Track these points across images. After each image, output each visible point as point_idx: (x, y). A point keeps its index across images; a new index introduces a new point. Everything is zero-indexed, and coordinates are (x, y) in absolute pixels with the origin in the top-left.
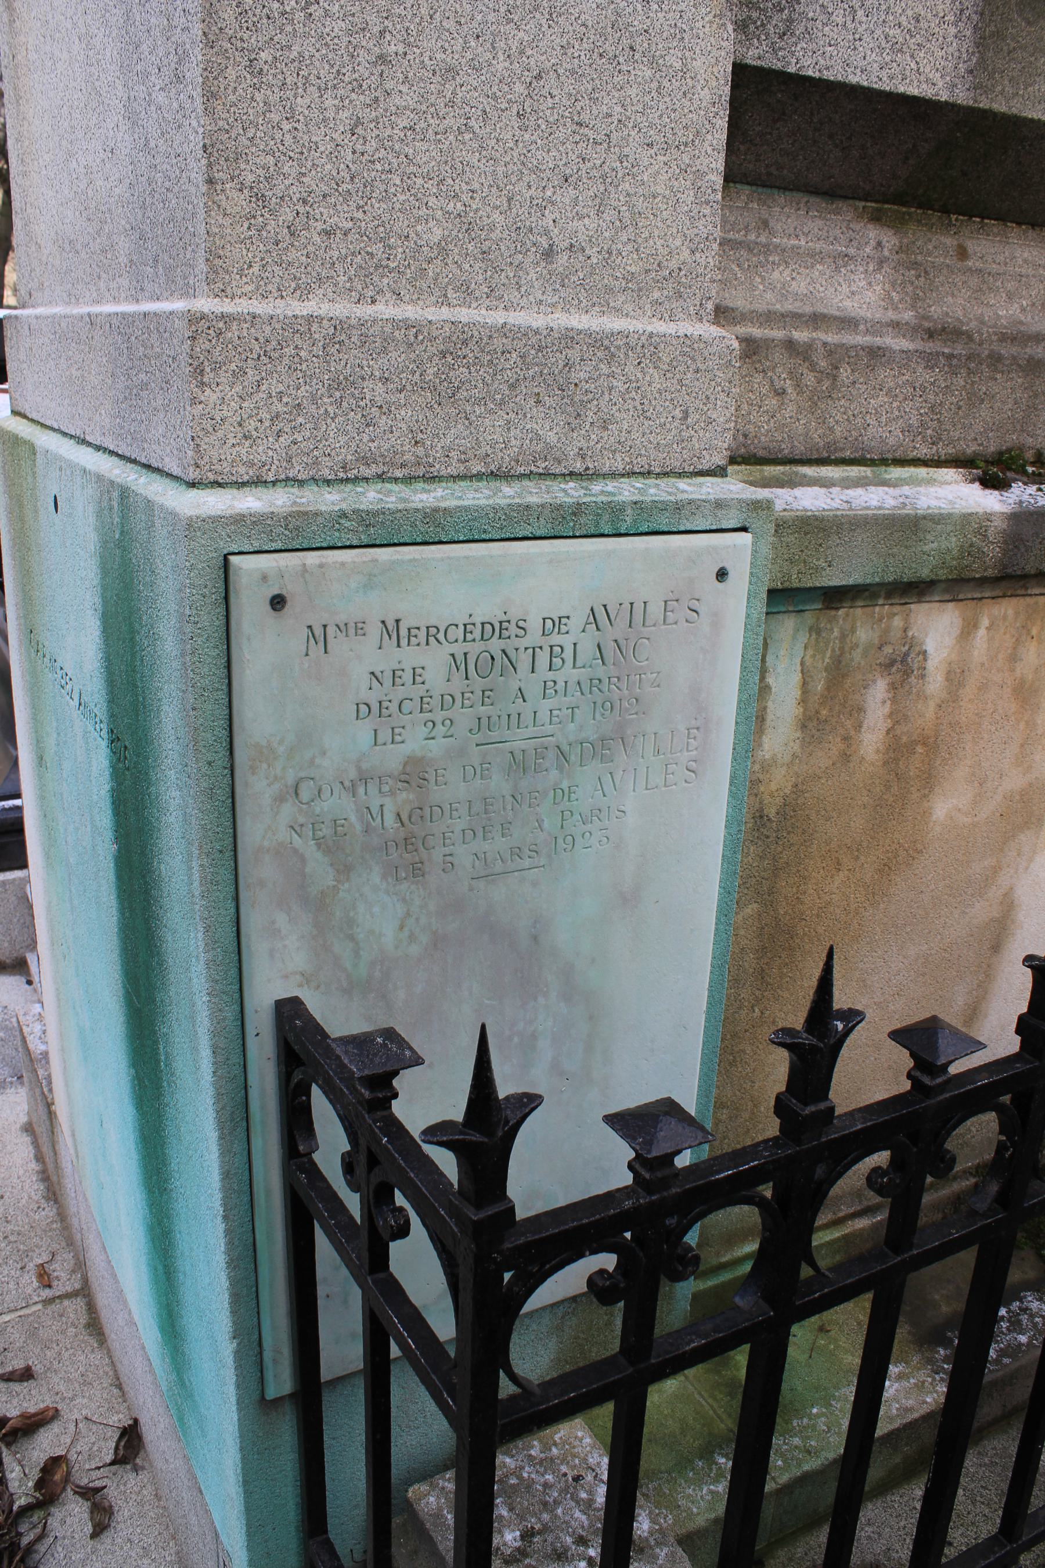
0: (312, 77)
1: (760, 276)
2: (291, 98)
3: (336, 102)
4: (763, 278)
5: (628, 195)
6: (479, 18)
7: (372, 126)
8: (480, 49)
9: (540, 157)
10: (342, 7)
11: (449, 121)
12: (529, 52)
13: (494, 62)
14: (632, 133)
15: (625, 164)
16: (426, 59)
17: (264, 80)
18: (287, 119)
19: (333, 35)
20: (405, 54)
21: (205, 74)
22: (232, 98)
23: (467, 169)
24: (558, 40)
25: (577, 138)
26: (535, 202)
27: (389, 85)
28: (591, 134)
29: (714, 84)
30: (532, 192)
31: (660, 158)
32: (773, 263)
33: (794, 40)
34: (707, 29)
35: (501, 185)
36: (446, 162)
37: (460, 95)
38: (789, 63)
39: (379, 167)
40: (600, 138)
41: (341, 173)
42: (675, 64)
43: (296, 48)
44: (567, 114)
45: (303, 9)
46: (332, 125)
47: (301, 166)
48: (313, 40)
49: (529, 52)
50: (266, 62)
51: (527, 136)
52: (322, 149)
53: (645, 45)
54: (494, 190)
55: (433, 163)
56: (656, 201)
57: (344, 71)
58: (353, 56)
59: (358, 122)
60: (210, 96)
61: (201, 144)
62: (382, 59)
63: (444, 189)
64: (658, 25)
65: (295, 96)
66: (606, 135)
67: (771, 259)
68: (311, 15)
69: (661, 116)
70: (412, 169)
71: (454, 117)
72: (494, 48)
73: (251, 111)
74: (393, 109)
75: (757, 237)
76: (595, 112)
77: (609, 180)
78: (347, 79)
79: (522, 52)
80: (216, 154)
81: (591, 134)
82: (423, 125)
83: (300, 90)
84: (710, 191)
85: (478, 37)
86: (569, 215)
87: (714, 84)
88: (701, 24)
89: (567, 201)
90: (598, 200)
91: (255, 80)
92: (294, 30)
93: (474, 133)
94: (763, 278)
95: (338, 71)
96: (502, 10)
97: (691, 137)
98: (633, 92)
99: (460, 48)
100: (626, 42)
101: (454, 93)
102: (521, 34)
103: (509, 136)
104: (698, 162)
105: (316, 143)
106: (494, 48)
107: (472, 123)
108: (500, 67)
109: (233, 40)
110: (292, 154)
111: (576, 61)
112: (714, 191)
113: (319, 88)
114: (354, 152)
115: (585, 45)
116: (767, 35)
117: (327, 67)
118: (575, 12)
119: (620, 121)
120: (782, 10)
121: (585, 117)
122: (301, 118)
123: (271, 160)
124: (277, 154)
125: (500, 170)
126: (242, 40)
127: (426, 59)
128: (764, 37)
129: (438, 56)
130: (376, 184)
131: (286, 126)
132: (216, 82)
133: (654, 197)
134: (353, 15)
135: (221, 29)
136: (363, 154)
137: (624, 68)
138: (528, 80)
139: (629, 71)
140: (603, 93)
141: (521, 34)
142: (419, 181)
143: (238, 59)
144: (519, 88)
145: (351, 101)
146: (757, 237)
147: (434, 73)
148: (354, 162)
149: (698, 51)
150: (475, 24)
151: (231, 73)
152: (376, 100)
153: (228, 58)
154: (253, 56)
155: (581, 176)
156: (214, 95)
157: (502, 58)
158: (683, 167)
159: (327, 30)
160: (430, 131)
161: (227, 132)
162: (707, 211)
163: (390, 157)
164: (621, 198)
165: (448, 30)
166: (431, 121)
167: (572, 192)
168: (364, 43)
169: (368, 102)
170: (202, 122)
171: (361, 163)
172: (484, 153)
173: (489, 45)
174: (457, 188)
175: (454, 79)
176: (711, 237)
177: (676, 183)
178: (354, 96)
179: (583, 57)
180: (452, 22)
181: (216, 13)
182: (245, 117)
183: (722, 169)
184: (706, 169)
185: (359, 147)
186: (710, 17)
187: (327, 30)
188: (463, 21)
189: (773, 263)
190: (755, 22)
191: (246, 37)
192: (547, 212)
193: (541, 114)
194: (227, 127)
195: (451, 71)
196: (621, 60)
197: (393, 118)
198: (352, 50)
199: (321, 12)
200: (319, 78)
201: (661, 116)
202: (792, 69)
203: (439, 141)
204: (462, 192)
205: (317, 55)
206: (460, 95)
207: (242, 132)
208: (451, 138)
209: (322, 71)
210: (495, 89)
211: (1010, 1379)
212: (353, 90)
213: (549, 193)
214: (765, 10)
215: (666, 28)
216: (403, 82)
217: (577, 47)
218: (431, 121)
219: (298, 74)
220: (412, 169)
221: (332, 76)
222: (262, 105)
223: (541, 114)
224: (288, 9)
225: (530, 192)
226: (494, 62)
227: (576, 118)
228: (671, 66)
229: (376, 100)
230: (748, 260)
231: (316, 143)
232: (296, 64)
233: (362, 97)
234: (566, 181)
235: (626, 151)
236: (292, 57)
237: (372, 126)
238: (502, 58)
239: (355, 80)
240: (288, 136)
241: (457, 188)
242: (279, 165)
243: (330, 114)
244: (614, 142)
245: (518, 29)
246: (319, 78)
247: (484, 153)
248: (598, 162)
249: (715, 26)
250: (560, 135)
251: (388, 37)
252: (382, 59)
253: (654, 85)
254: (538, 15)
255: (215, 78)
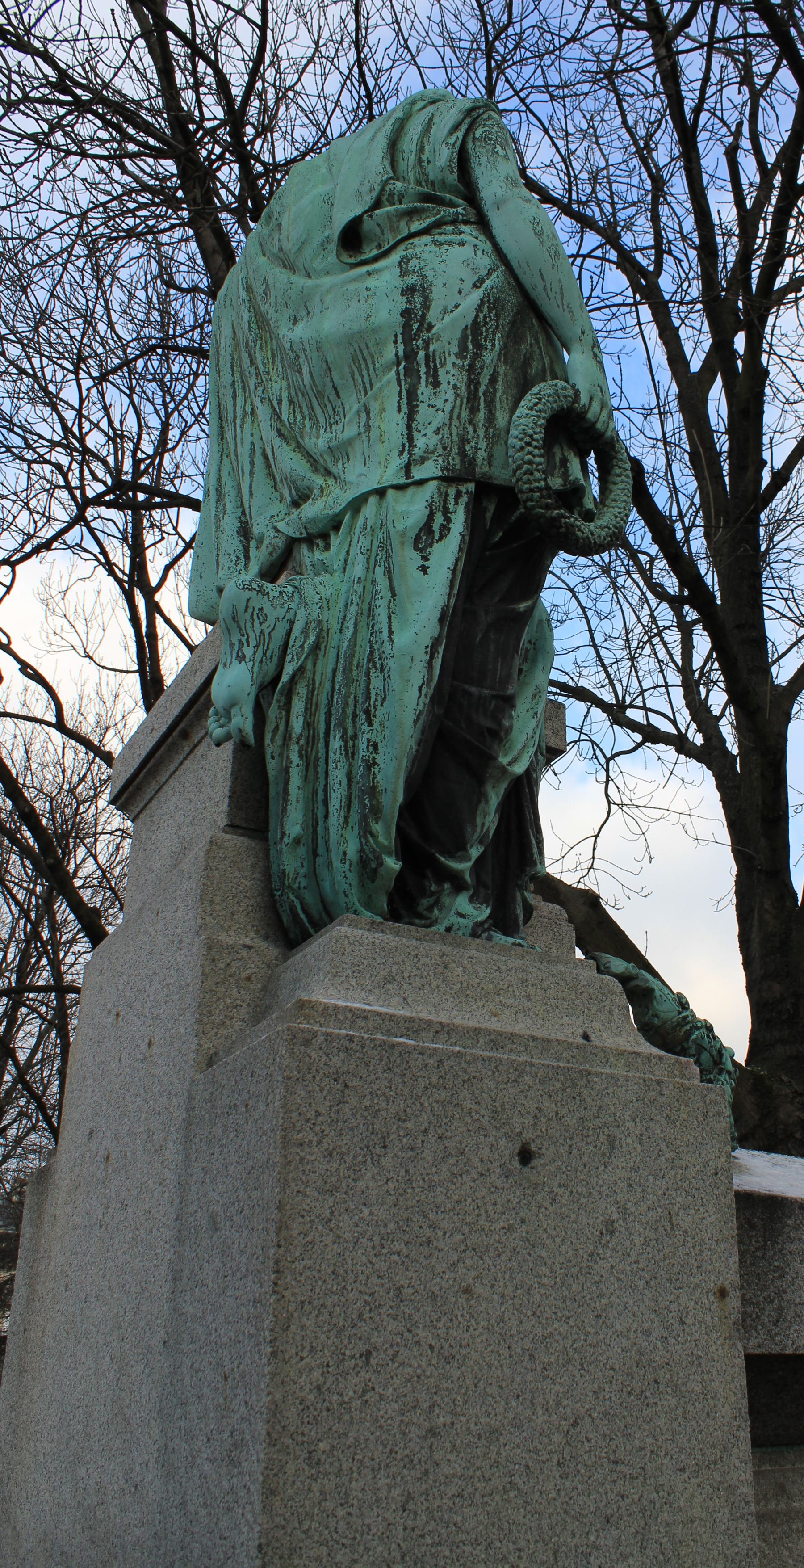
0: (366, 1459)
1: (787, 1548)
2: (347, 1483)
3: (388, 1481)
4: (790, 1550)
5: (668, 1525)
6: (518, 1379)
7: (422, 1499)
8: (521, 1407)
9: (581, 1503)
10: (395, 1390)
11: (496, 1482)
12: (565, 1402)
13: (534, 1417)
14: (665, 1461)
15: (661, 1493)
16: (472, 1426)
17: (321, 1469)
18: (342, 1505)
19: (387, 1416)
20: (453, 1424)
21: (266, 1472)
22: (290, 1492)
23: (513, 1528)
24: (590, 1387)
25: (615, 1476)
26: (580, 1551)
27: (438, 1455)
28: (627, 1470)
29: (733, 1399)
30: (576, 1540)
31: (694, 1481)
32: (797, 1531)
33: (787, 1324)
34: (720, 1351)
35: (547, 1538)
36: (493, 1525)
37: (504, 1454)
38: (785, 1346)
39: (429, 1540)
40: (635, 1472)
41: (393, 1554)
42: (696, 1388)
43: (352, 1434)
44: (603, 1455)
45: (361, 1397)
46: (384, 1505)
47: (353, 1552)
48: (368, 1424)
49: (565, 1402)
50: (324, 1452)
51: (568, 1484)
52: (374, 1530)
53: (668, 1376)
54: (540, 1545)
55: (481, 1527)
56: (695, 1525)
57: (397, 1449)
58: (404, 1434)
59: (410, 1497)
60: (270, 1492)
61: (256, 1543)
62: (432, 1432)
63: (491, 1552)
64: (676, 1357)
65: (350, 1482)
66: (641, 1468)
67: (794, 1527)
68: (367, 1401)
69: (689, 1439)
70: (462, 1536)
71: (500, 1476)
72: (533, 1404)
73: (307, 1502)
74: (442, 1479)
75: (777, 1505)
76: (629, 1448)
77: (648, 1513)
78: (399, 1456)
79: (558, 1404)
80: (270, 1553)
81: (627, 1470)
82: (470, 1489)
83: (355, 1474)
84: (743, 1504)
85: (518, 1396)
86: (614, 1557)
87: (733, 1399)
88: (714, 1347)
89: (610, 1543)
90: (639, 1537)
91: (313, 1471)
92: (352, 1418)
93: (518, 1489)
94: (790, 1550)
95: (391, 1451)
96: (539, 1368)
97: (719, 1454)
98: (661, 1422)
99: (502, 1410)
100: (650, 1377)
101: (499, 1453)
102: (557, 1387)
103: (551, 1486)
104: (728, 1477)
105: (369, 1526)
106: (533, 1404)
107: (517, 1480)
108: (539, 1421)
109: (295, 1436)
110: (344, 1541)
111: (608, 1403)
112: (747, 1503)
113: (373, 1470)
114: (405, 1529)
115: (614, 1387)
116: (763, 1325)
117: (380, 1448)
118: (603, 1359)
119: (652, 1452)
120: (772, 1301)
121: (620, 1454)
122: (355, 1502)
123: (324, 1550)
124: (330, 1543)
125: (545, 1522)
126: (303, 1434)
127: (472, 1426)
128: (760, 1327)
129: (482, 1420)
130: (426, 1559)
131: (341, 1512)
132: (275, 1479)
133: (692, 1522)
134: (405, 1395)
135: (284, 1427)
136: (413, 1530)
137: (652, 1401)
138: (566, 1429)
139: (656, 1403)
140: (634, 1428)
141: (557, 1387)
142: (468, 1549)
143: (298, 1453)
144: (557, 1438)
145: (402, 1478)
146: (777, 1505)
147: (479, 1438)
148: (405, 1540)
149: (715, 1373)
150: (515, 1385)
151: (291, 1468)
152: (426, 1472)
153: (289, 1454)
154: (313, 1448)
155: (621, 1515)
156: (273, 1492)
157: (540, 1412)
158: (715, 1485)
159: (382, 1413)
160: (477, 1495)
161: (283, 1527)
162: (743, 1525)
163: (439, 1528)
164: (662, 1530)
165: (491, 1396)
166: (478, 1485)
167: (614, 1532)
168: (415, 1420)
169: (419, 1475)
170: (259, 1521)
171: (412, 1538)
172: (529, 1508)
173: (528, 1402)
174: (505, 1549)
175: (498, 1439)
176: (751, 1553)
177: (711, 1503)
178: (405, 1471)
179: (613, 1398)
180: (494, 1387)
181: (281, 1412)
182: (301, 1510)
183: (751, 1479)
184: (737, 1483)
185: (410, 1522)
186: (721, 1340)
187: (382, 1413)
188: (504, 1384)
189: (797, 1531)
190: (751, 1316)
191: (306, 1430)
192: (592, 1558)
193: (579, 1459)
194: (283, 1523)
195: (495, 1432)
196: (648, 1394)
197: (442, 1487)
198: (403, 1428)
199: (377, 1397)
200: (373, 1459)
201: (689, 1439)
202: (789, 1351)
203: (486, 1503)
204: (510, 1553)
205: (372, 1438)
206: (504, 1454)
207: (297, 1525)
208: (497, 1498)
209: (376, 1453)
210: (536, 1442)
211: (232, 704)
212: (405, 1467)
213: (592, 1538)
214: (758, 1304)
215: (684, 1357)
216: (451, 1451)
217: (607, 1389)
218: (478, 1485)
219: (353, 1459)
220: (462, 1536)
221: (385, 1456)
222: (318, 1494)
223: (579, 1459)
224: (346, 1399)
225: (575, 1541)
226: (534, 1417)
227: (612, 1457)
228: (693, 1391)
229: (426, 1472)
230: (773, 1533)
231: (369, 1526)
232: (352, 1449)
233: (413, 1473)
234: (608, 1522)
235: (661, 1480)
236: (348, 1443)
237: (422, 1499)
238: (540, 1412)
239: (407, 1456)
240: (341, 1523)
241: (505, 1549)
242: (332, 1555)
243: (383, 1494)
244: (649, 1473)
245: (554, 1383)
246: (373, 1459)
247: (529, 1508)
248: (636, 1497)
249: (726, 1347)
250: (599, 1476)
251: (437, 1411)
252: (432, 1432)
253: (680, 1411)
254: (570, 1367)
255: (276, 1475)
